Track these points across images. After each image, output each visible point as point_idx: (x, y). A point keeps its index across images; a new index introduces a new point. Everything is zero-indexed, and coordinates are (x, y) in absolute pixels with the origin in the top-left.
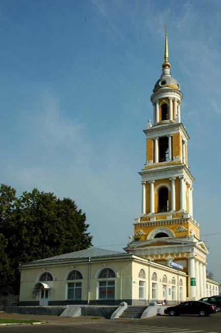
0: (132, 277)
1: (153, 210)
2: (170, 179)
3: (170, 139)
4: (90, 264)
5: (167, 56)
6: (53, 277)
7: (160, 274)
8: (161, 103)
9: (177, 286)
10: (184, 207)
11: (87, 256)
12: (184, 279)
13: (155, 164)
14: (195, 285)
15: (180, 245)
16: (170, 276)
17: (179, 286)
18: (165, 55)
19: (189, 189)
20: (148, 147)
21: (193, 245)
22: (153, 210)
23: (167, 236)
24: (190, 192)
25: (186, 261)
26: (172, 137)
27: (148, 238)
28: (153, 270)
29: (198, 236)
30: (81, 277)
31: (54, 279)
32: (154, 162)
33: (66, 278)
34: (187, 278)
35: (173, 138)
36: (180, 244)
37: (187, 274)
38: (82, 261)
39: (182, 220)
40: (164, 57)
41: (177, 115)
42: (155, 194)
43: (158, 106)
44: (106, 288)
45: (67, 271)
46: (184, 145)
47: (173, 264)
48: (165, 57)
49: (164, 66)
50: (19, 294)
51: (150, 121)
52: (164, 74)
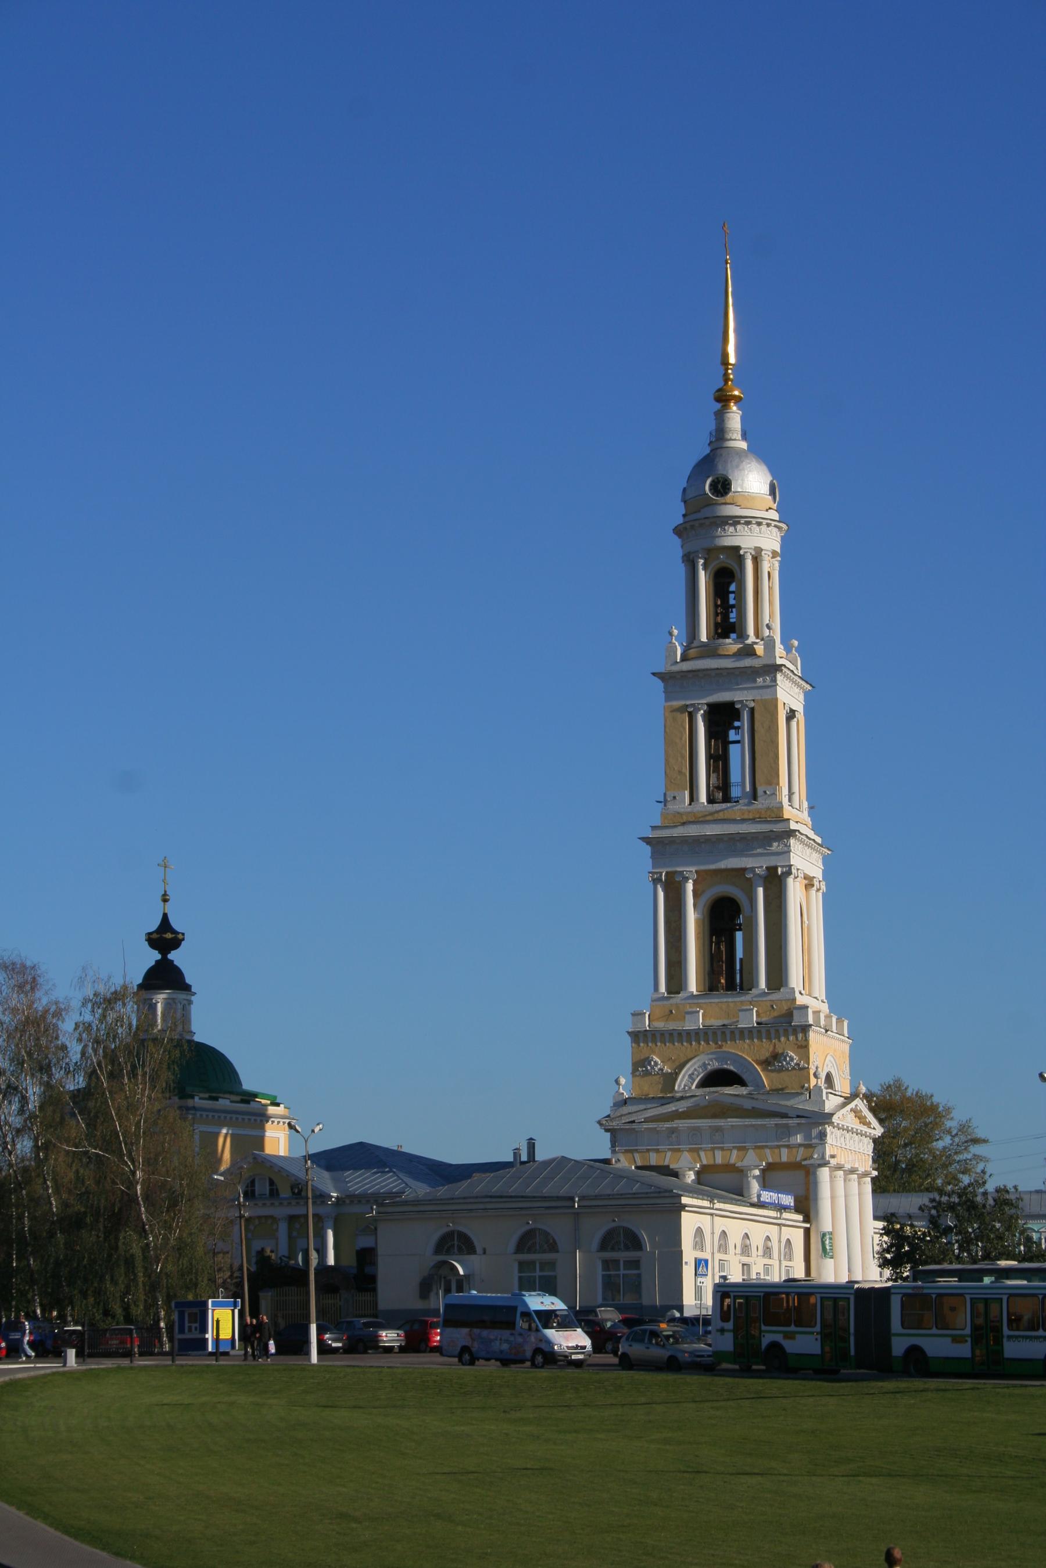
0: (681, 1252)
1: (693, 985)
2: (749, 875)
4: (578, 1214)
5: (732, 360)
6: (476, 1243)
7: (735, 1229)
8: (714, 565)
9: (776, 1263)
10: (795, 978)
11: (563, 1192)
12: (797, 1237)
13: (696, 808)
14: (832, 1258)
15: (784, 1121)
16: (758, 1233)
17: (784, 1263)
18: (725, 355)
19: (813, 891)
20: (669, 742)
21: (774, 669)
22: (693, 985)
23: (742, 1083)
24: (817, 900)
25: (800, 1175)
26: (752, 711)
27: (681, 1082)
28: (721, 1224)
29: (843, 1085)
30: (553, 1247)
31: (479, 1250)
32: (692, 799)
33: (512, 1246)
34: (807, 1232)
35: (756, 715)
36: (785, 1116)
37: (807, 1219)
38: (554, 1204)
39: (789, 1025)
40: (719, 361)
41: (768, 627)
42: (697, 921)
43: (702, 576)
44: (619, 1275)
45: (514, 1230)
46: (794, 723)
47: (767, 1196)
48: (725, 362)
49: (723, 399)
50: (374, 1290)
51: (675, 632)
52: (720, 433)
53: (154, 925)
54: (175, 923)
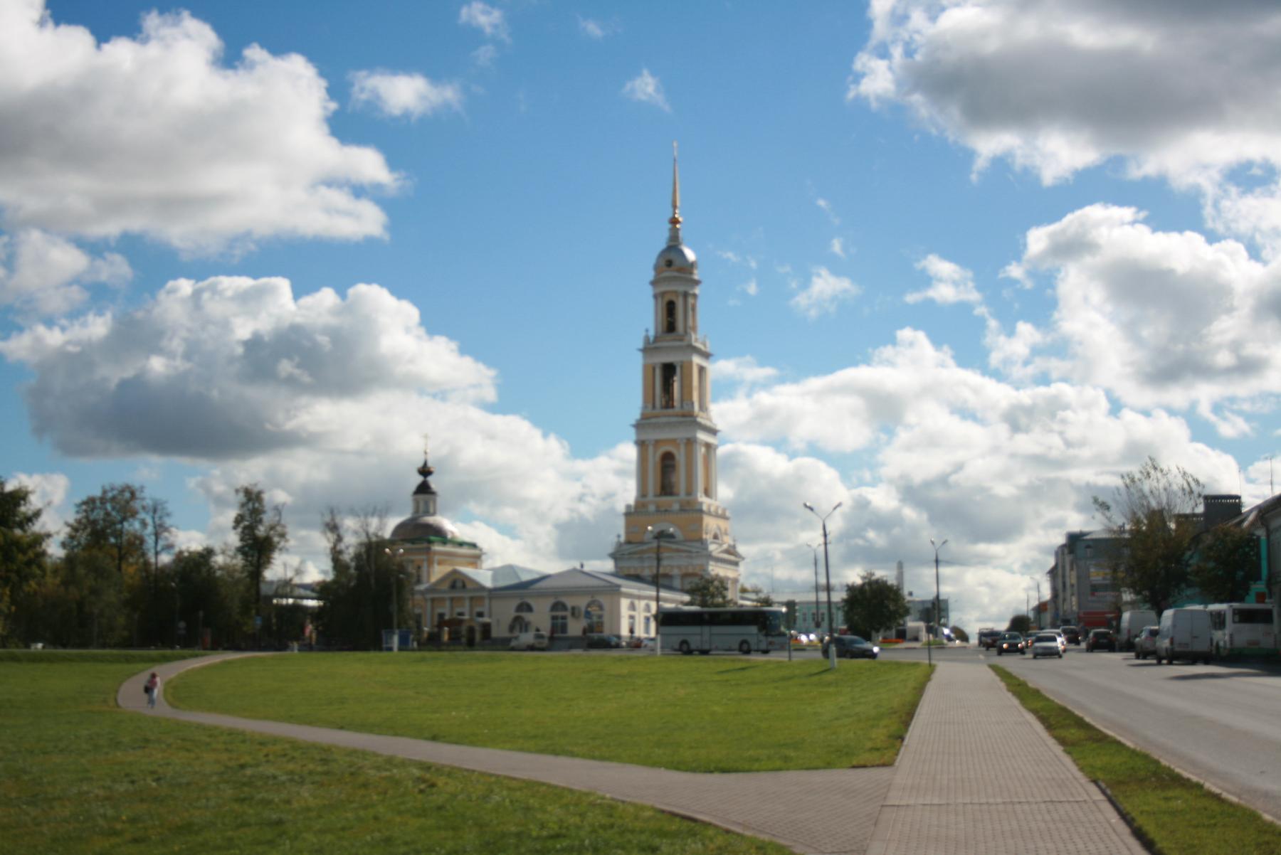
1: (651, 497)
3: (678, 370)
32: (654, 407)
45: (551, 601)
53: (420, 464)
54: (430, 464)
